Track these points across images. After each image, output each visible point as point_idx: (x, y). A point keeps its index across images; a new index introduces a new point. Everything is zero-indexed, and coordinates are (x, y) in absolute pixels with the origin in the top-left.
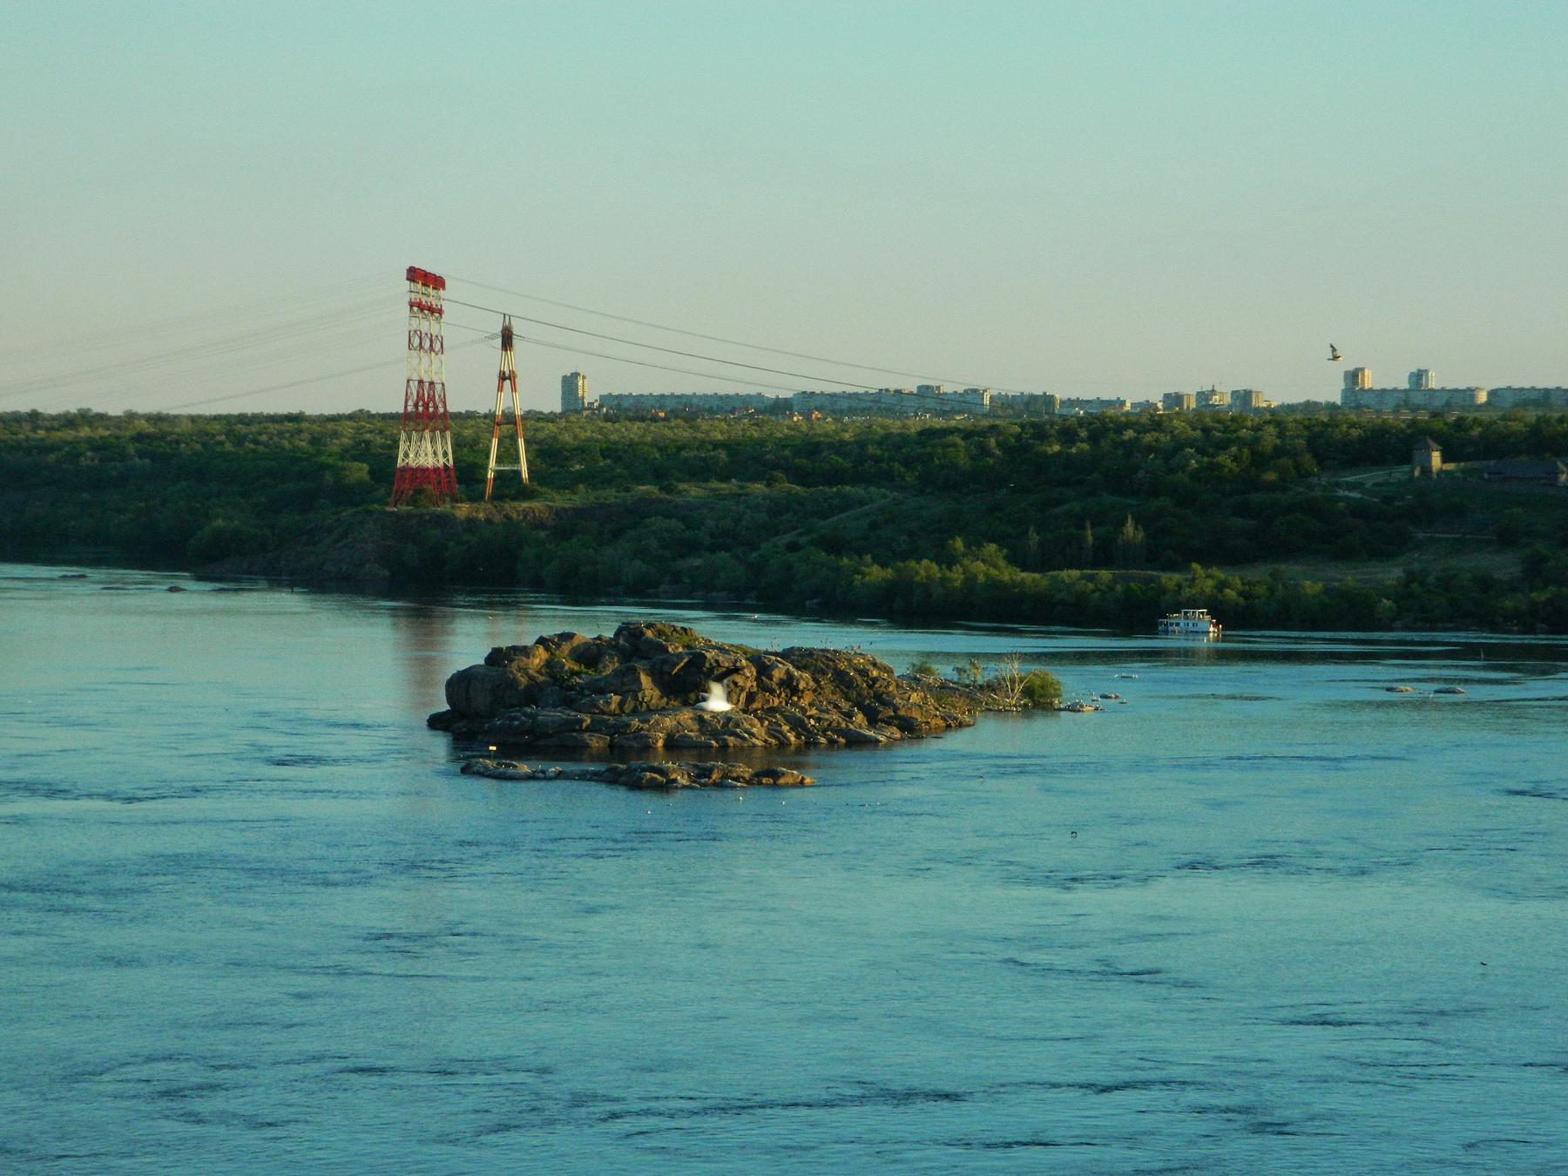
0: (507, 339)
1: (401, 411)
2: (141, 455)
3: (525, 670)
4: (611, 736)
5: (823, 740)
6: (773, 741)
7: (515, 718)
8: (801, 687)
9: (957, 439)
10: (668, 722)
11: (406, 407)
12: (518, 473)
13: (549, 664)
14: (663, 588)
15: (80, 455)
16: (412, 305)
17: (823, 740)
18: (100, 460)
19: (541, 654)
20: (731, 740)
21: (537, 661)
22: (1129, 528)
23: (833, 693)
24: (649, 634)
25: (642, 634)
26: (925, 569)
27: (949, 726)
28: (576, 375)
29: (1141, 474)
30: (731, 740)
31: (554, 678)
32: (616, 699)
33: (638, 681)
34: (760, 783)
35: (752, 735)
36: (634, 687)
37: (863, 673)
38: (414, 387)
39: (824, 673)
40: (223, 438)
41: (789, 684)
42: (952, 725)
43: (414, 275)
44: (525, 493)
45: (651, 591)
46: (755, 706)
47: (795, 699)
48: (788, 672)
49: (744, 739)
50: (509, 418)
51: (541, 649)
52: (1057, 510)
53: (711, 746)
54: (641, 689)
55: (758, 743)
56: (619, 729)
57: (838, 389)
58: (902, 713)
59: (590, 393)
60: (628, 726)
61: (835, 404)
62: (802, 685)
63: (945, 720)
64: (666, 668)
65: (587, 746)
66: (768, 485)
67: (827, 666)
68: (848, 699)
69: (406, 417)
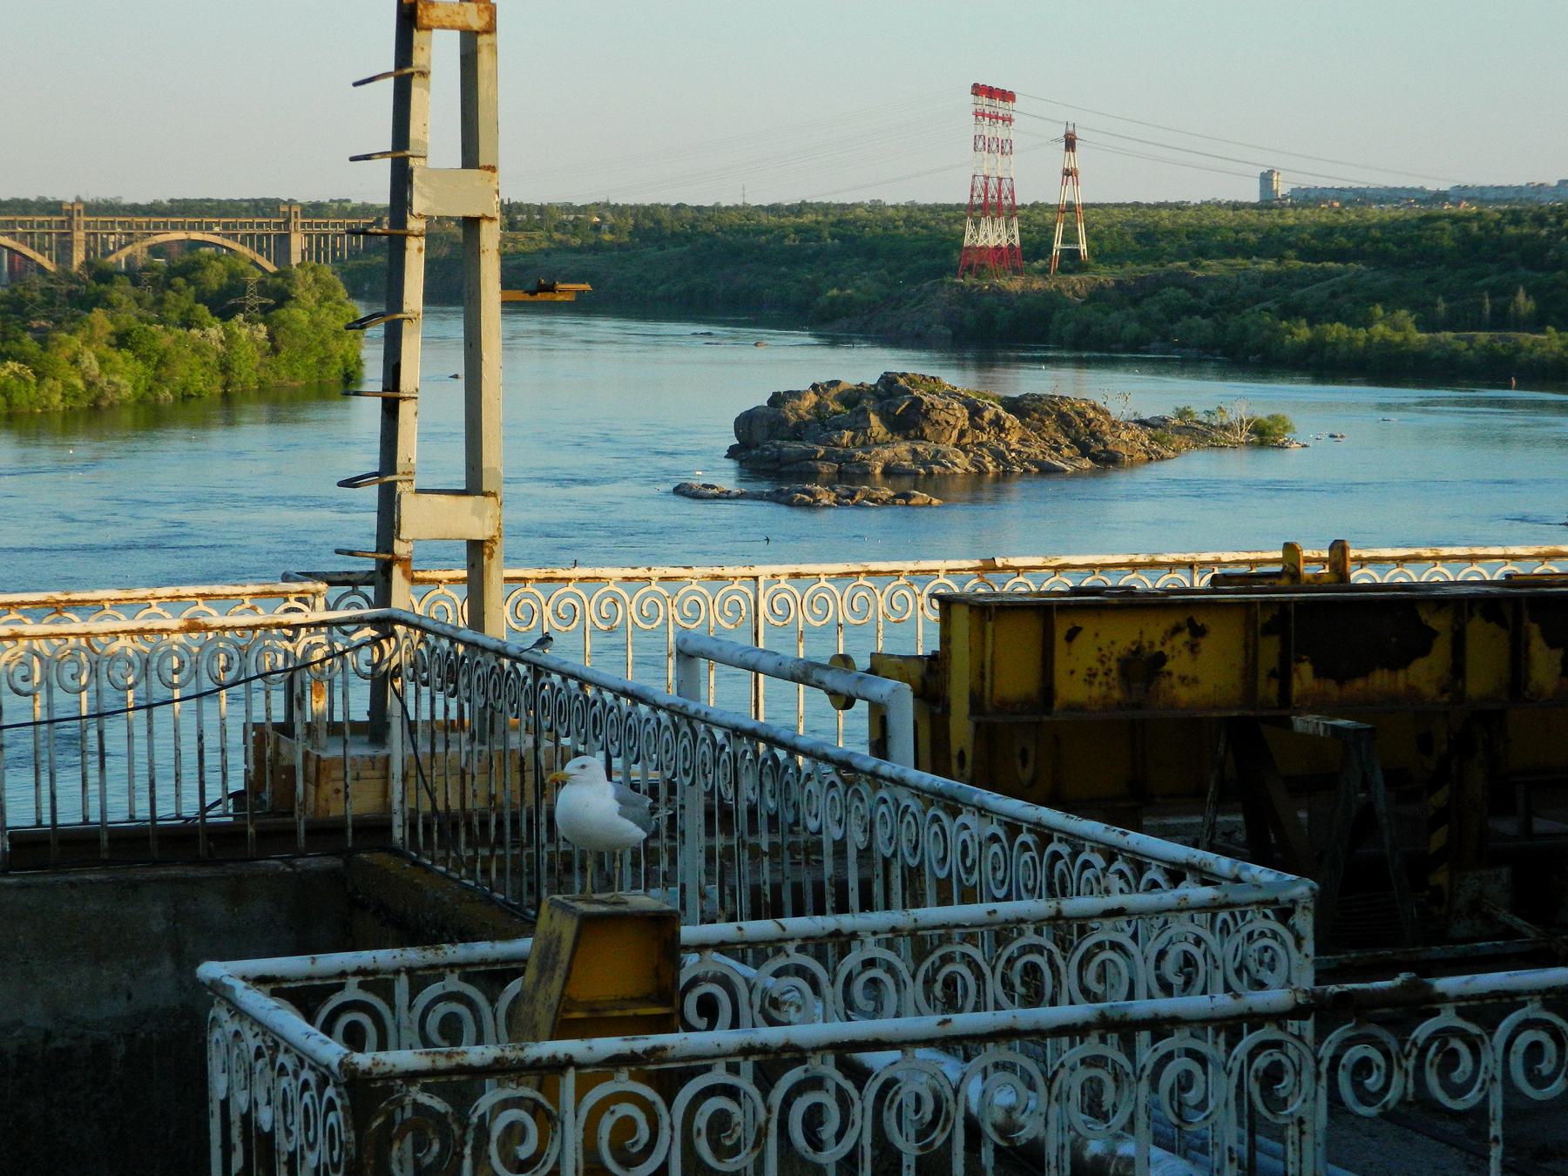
0: (1070, 143)
1: (966, 201)
2: (833, 236)
3: (795, 410)
4: (840, 464)
5: (1017, 469)
6: (973, 470)
7: (767, 449)
8: (1007, 426)
9: (1445, 224)
10: (887, 454)
11: (972, 197)
12: (1078, 251)
13: (817, 406)
14: (1152, 345)
15: (786, 236)
16: (976, 114)
17: (1017, 469)
18: (801, 241)
19: (812, 398)
20: (936, 469)
21: (807, 403)
22: (1521, 297)
23: (1056, 431)
24: (902, 382)
25: (897, 382)
26: (1337, 331)
27: (1151, 459)
28: (1271, 172)
29: (1551, 253)
30: (936, 469)
31: (819, 418)
32: (848, 434)
33: (868, 419)
34: (894, 503)
35: (954, 464)
36: (865, 425)
37: (1081, 414)
38: (980, 182)
39: (1049, 414)
40: (901, 223)
41: (997, 423)
42: (1152, 457)
43: (978, 90)
44: (1082, 267)
45: (1143, 347)
46: (965, 441)
47: (1003, 435)
48: (997, 414)
49: (947, 467)
50: (1071, 207)
51: (812, 394)
52: (1480, 283)
53: (918, 474)
54: (869, 426)
55: (959, 471)
56: (848, 458)
57: (1346, 185)
58: (1110, 447)
59: (1282, 187)
60: (853, 456)
61: (1480, 195)
62: (1008, 425)
63: (1148, 454)
64: (891, 410)
65: (820, 472)
66: (1279, 262)
67: (1053, 409)
68: (1067, 436)
69: (971, 208)
